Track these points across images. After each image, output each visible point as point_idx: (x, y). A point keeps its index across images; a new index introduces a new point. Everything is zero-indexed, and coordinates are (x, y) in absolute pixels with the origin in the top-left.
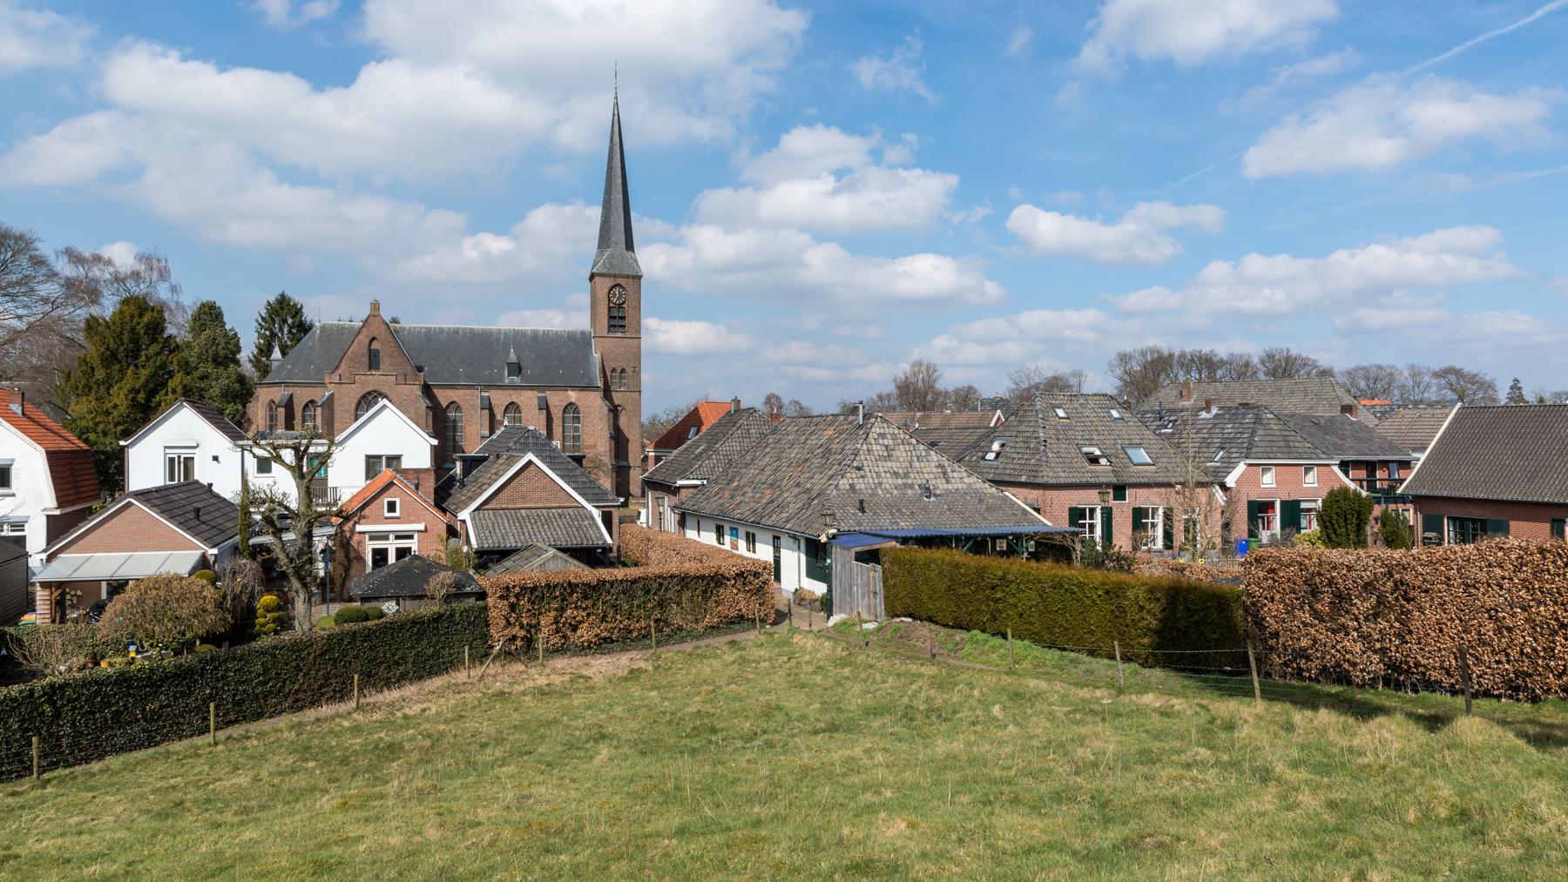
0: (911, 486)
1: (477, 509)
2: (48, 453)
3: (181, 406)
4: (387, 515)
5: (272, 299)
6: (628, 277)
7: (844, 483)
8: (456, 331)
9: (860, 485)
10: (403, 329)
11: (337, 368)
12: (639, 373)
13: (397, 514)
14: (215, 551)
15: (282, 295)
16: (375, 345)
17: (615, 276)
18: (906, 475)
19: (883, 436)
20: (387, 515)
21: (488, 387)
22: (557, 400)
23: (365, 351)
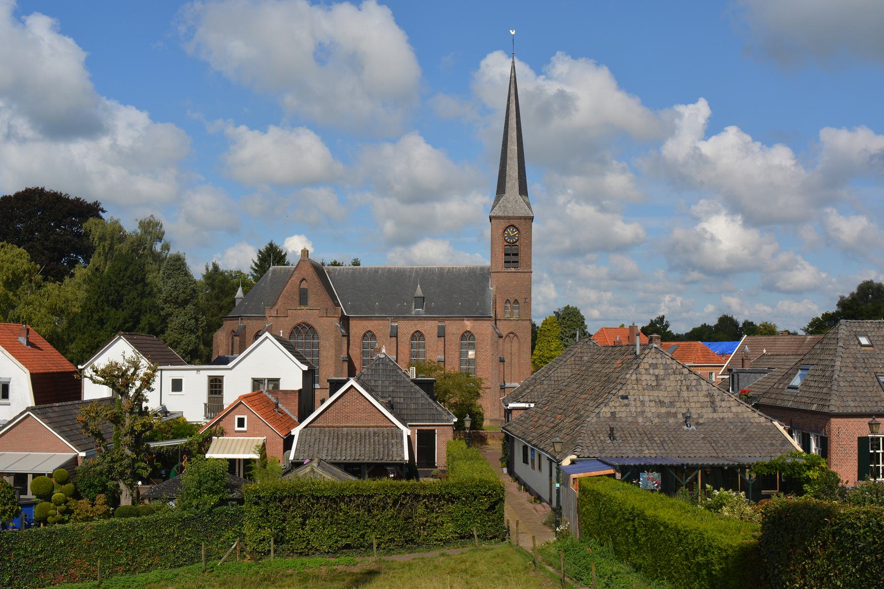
0: (675, 415)
1: (306, 427)
2: (31, 374)
3: (120, 338)
4: (237, 429)
5: (263, 248)
6: (520, 218)
7: (605, 411)
8: (376, 271)
9: (622, 413)
10: (365, 270)
11: (275, 304)
12: (530, 304)
13: (245, 429)
14: (83, 454)
15: (271, 245)
16: (304, 285)
17: (509, 218)
18: (672, 404)
19: (655, 366)
20: (237, 429)
21: (396, 319)
22: (454, 328)
23: (297, 290)
